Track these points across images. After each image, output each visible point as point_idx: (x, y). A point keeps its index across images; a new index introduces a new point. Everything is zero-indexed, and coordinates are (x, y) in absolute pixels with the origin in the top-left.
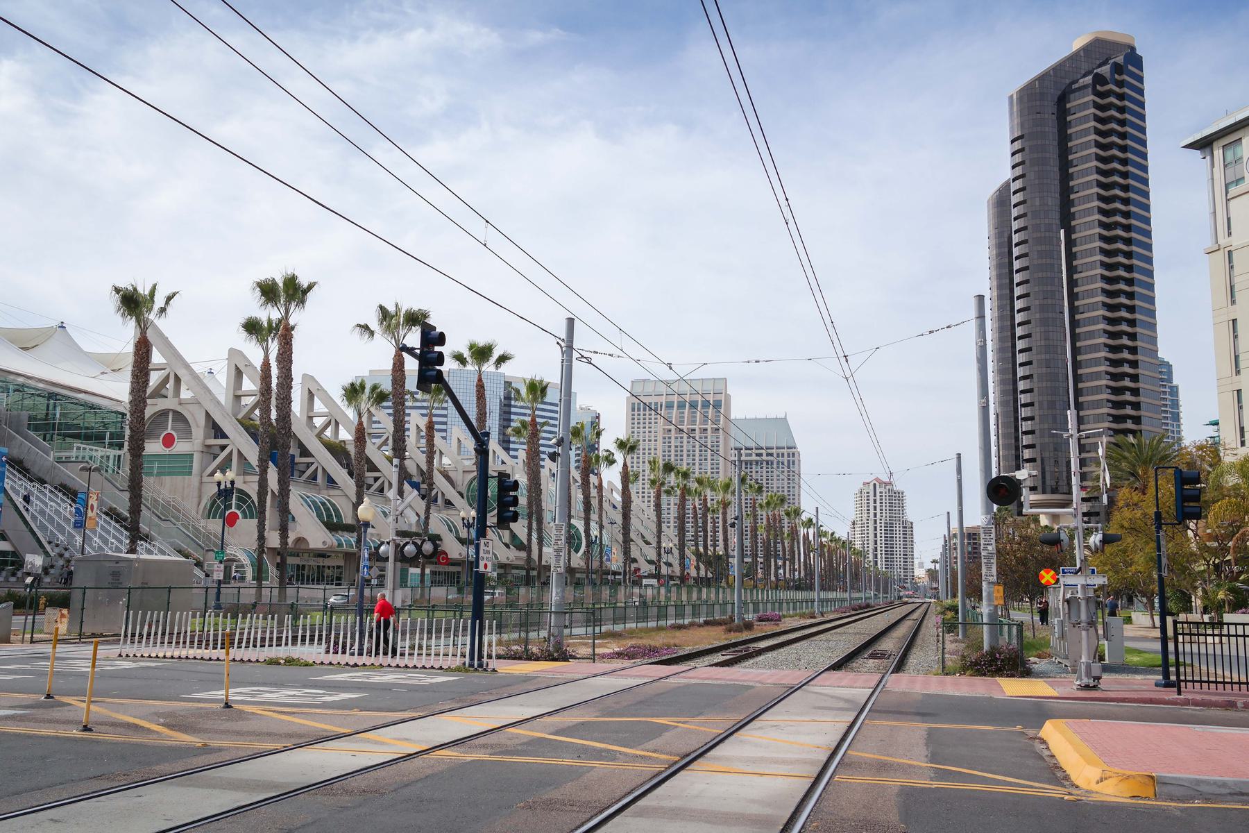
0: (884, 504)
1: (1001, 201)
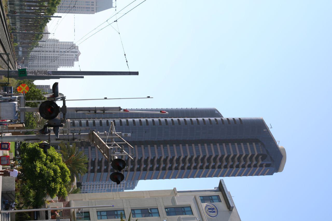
0: (70, 56)
1: (213, 113)
